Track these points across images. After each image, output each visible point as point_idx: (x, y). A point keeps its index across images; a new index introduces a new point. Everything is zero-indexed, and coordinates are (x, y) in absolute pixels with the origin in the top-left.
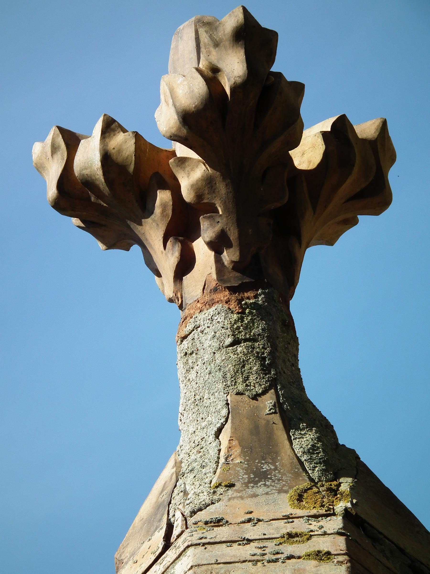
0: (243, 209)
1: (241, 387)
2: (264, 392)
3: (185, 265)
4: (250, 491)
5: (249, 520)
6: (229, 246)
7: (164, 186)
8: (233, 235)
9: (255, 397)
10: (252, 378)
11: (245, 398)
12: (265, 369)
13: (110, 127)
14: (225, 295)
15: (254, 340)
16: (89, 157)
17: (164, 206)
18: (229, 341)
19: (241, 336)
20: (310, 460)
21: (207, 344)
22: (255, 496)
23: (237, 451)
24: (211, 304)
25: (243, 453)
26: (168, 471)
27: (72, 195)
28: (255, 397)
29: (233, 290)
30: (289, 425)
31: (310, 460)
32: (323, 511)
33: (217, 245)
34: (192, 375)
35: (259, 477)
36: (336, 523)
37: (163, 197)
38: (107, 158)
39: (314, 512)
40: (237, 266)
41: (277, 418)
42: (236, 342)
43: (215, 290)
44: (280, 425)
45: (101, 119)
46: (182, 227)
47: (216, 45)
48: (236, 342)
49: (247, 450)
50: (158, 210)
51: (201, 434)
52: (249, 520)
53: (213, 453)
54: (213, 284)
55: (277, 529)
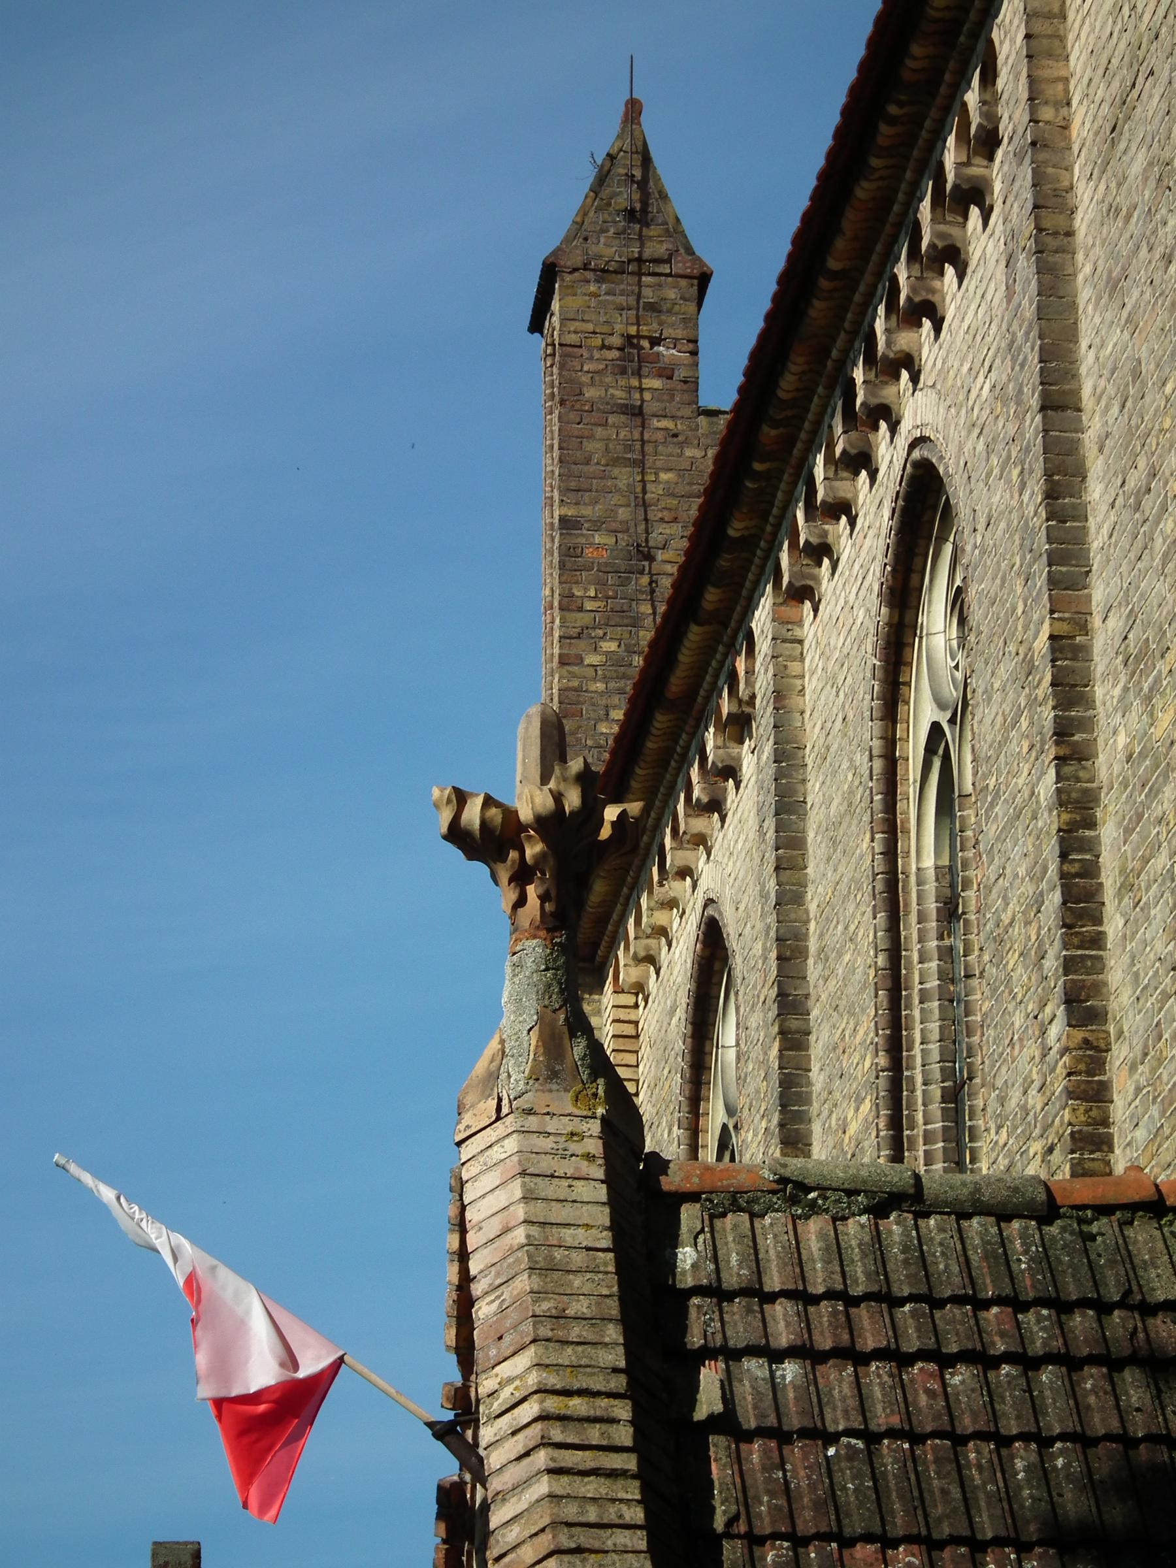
0: (560, 878)
1: (546, 1003)
2: (560, 1008)
3: (521, 902)
4: (548, 1086)
5: (548, 1114)
6: (550, 901)
7: (514, 849)
8: (553, 893)
9: (555, 1011)
10: (554, 996)
11: (548, 1011)
12: (562, 991)
13: (489, 801)
14: (543, 933)
15: (557, 969)
16: (473, 814)
17: (513, 861)
18: (543, 967)
19: (550, 965)
20: (582, 1065)
21: (529, 964)
22: (551, 1091)
23: (541, 1050)
24: (535, 937)
25: (545, 1054)
26: (494, 1045)
27: (456, 834)
28: (555, 1011)
29: (549, 930)
30: (572, 1035)
31: (582, 1065)
32: (590, 1114)
33: (543, 898)
34: (516, 980)
35: (553, 1075)
36: (595, 1127)
37: (513, 855)
38: (484, 823)
39: (585, 1113)
40: (552, 914)
41: (565, 1029)
42: (547, 969)
43: (538, 928)
44: (567, 1035)
45: (483, 795)
46: (522, 877)
47: (565, 780)
48: (547, 969)
49: (547, 1052)
50: (509, 862)
51: (518, 1027)
52: (548, 1114)
53: (526, 1045)
54: (538, 923)
55: (564, 1125)
